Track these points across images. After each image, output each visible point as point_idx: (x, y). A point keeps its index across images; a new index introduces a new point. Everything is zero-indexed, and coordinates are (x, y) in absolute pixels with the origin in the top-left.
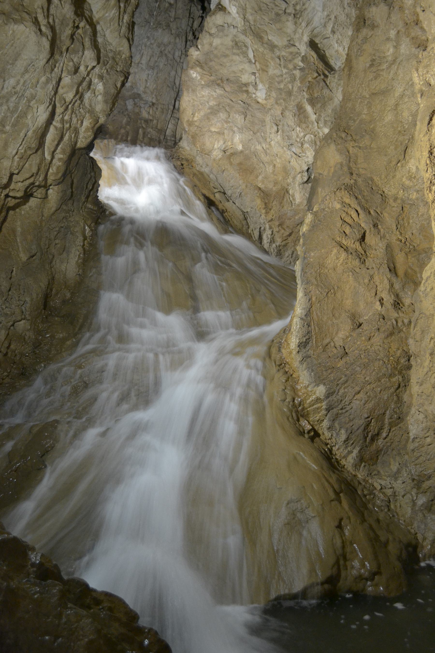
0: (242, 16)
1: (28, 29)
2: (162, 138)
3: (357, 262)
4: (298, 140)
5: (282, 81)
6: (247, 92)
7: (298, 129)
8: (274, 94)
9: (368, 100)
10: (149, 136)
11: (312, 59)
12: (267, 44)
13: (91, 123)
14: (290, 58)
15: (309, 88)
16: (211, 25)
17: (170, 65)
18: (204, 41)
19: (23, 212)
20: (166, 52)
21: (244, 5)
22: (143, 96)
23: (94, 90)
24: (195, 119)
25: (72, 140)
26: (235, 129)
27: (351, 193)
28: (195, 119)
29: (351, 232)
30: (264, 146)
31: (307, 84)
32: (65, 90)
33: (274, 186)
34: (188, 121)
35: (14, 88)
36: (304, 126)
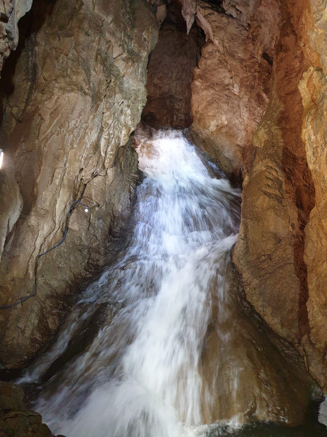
0: (222, 45)
1: (76, 94)
2: (187, 118)
3: (276, 203)
4: (259, 115)
5: (248, 80)
6: (228, 89)
7: (259, 108)
8: (243, 89)
9: (284, 98)
10: (180, 118)
11: (265, 65)
12: (238, 59)
13: (126, 132)
14: (252, 65)
15: (263, 83)
16: (205, 52)
17: (189, 76)
18: (203, 63)
19: (95, 184)
20: (186, 69)
21: (222, 38)
22: (175, 96)
23: (125, 114)
24: (199, 109)
25: (117, 142)
26: (223, 112)
27: (273, 159)
28: (199, 109)
29: (272, 184)
30: (240, 120)
31: (263, 81)
32: (107, 118)
33: (247, 143)
34: (195, 111)
35: (75, 125)
36: (262, 106)
